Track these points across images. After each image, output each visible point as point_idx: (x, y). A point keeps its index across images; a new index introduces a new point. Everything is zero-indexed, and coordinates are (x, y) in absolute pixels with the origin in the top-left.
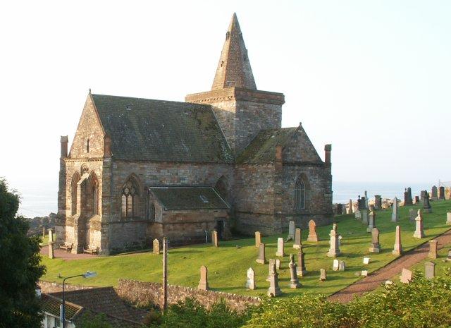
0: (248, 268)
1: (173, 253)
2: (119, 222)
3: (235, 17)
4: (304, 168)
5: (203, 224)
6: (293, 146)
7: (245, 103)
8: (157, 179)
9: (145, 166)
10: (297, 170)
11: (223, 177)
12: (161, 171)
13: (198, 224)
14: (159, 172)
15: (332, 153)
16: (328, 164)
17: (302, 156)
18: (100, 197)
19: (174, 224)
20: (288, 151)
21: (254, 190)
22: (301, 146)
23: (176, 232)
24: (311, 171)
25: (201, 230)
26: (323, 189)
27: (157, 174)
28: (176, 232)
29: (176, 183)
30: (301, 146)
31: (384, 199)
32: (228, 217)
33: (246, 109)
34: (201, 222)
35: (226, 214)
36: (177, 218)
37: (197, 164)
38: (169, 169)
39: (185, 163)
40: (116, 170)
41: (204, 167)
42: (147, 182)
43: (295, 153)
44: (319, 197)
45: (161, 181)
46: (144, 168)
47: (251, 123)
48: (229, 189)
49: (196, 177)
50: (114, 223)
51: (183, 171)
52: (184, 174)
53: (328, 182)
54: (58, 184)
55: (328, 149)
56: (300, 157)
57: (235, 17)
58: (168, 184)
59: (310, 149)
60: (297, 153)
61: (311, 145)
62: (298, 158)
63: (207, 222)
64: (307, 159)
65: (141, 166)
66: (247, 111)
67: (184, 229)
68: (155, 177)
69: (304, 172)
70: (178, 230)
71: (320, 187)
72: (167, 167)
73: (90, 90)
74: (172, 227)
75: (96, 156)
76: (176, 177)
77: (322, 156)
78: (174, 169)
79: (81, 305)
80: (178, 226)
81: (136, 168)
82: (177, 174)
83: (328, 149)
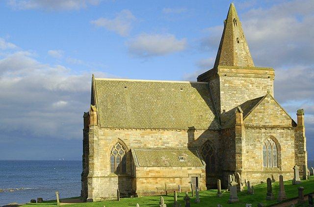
0: (251, 193)
2: (106, 177)
5: (176, 179)
10: (265, 133)
12: (145, 136)
13: (172, 179)
14: (143, 137)
17: (272, 121)
20: (255, 116)
23: (149, 185)
24: (282, 134)
25: (175, 184)
28: (149, 185)
29: (160, 146)
34: (174, 178)
35: (201, 172)
36: (150, 173)
37: (176, 129)
38: (152, 135)
40: (102, 135)
45: (146, 145)
48: (216, 152)
49: (180, 141)
58: (152, 147)
63: (181, 178)
67: (157, 183)
70: (144, 183)
74: (145, 181)
75: (272, 204)
76: (160, 141)
78: (158, 134)
80: (151, 180)
81: (122, 134)
82: (161, 139)
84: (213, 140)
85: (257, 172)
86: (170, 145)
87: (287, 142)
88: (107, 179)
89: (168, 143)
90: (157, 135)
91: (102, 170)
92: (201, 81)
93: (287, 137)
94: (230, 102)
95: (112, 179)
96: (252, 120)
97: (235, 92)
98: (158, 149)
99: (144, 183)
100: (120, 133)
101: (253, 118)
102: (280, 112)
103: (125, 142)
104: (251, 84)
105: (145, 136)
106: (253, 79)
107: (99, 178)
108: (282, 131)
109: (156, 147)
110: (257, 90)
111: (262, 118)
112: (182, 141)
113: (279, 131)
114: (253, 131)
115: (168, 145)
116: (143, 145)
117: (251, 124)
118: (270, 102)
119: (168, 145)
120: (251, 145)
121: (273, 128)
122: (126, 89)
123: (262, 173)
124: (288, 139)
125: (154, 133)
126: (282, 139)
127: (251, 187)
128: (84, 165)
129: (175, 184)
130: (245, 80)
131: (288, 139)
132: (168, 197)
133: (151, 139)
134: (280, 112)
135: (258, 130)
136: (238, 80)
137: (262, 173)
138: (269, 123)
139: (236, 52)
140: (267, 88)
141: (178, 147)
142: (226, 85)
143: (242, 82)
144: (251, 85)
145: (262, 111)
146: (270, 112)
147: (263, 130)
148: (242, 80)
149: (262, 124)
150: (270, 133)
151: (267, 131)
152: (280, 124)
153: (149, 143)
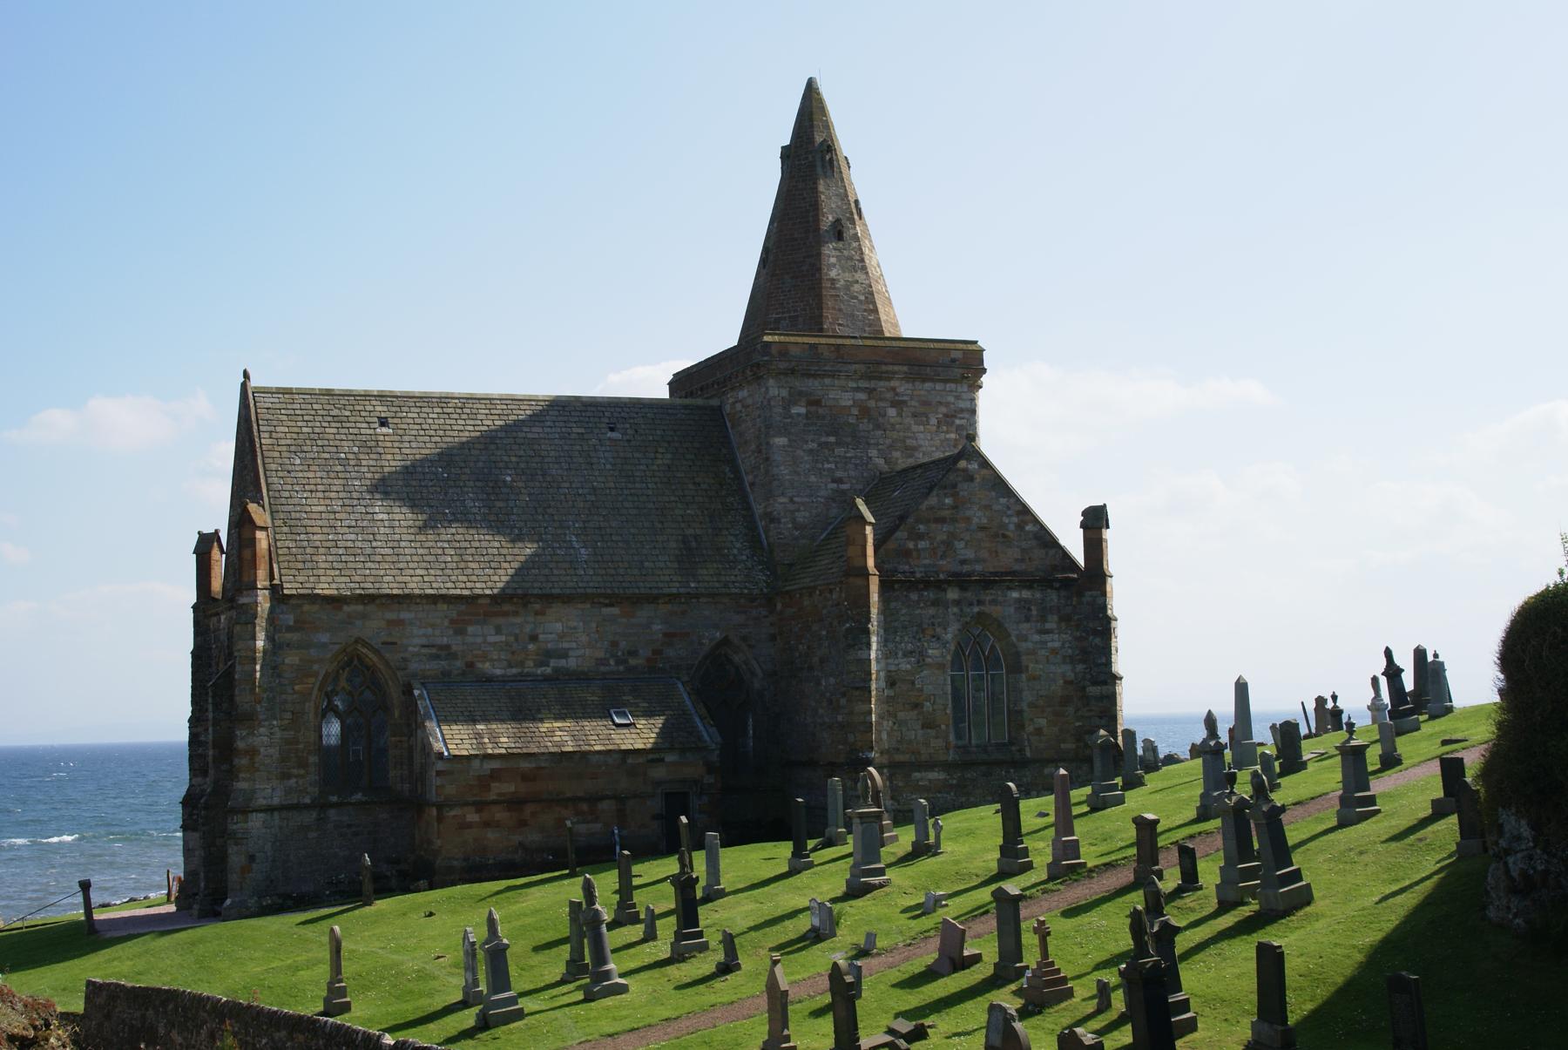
1: (905, 866)
2: (306, 807)
3: (811, 110)
4: (987, 596)
5: (605, 805)
6: (942, 520)
7: (813, 385)
8: (452, 656)
9: (405, 615)
10: (957, 603)
11: (725, 641)
12: (470, 629)
13: (585, 807)
14: (461, 632)
15: (1112, 537)
16: (1094, 575)
17: (984, 554)
19: (480, 806)
20: (920, 537)
21: (818, 683)
22: (978, 517)
24: (1023, 605)
25: (597, 827)
26: (1080, 667)
27: (456, 644)
28: (491, 835)
30: (978, 517)
31: (1213, 711)
32: (709, 779)
37: (612, 600)
38: (500, 620)
39: (567, 599)
40: (289, 629)
41: (644, 613)
42: (414, 666)
43: (948, 544)
44: (1065, 701)
45: (471, 665)
46: (400, 622)
47: (839, 451)
48: (757, 685)
49: (614, 644)
50: (281, 808)
51: (559, 627)
52: (562, 636)
54: (190, 691)
55: (1095, 520)
56: (969, 553)
57: (811, 110)
58: (498, 672)
59: (1020, 527)
60: (959, 545)
61: (1025, 511)
62: (963, 562)
64: (1008, 558)
65: (391, 616)
67: (523, 823)
68: (445, 652)
69: (987, 609)
71: (1071, 660)
73: (246, 375)
74: (472, 817)
76: (531, 647)
77: (1073, 543)
80: (500, 814)
82: (534, 638)
83: (1095, 520)
84: (744, 639)
85: (929, 765)
86: (572, 663)
87: (1046, 637)
88: (310, 817)
89: (564, 654)
90: (518, 620)
91: (285, 776)
92: (691, 395)
93: (1043, 619)
94: (813, 478)
95: (332, 813)
96: (907, 554)
97: (832, 439)
98: (521, 678)
99: (470, 826)
100: (364, 616)
101: (911, 545)
103: (387, 655)
104: (894, 404)
105: (470, 629)
106: (903, 388)
107: (276, 814)
108: (1026, 594)
109: (514, 671)
110: (915, 428)
112: (623, 644)
114: (914, 596)
115: (562, 663)
116: (459, 663)
117: (907, 568)
118: (978, 479)
119: (562, 663)
120: (905, 655)
121: (987, 582)
122: (384, 430)
123: (947, 766)
124: (1048, 626)
125: (505, 614)
127: (1515, 874)
128: (1075, 908)
129: (597, 827)
130: (870, 391)
131: (1048, 626)
132: (404, 580)
133: (491, 639)
134: (1015, 519)
135: (930, 595)
136: (844, 389)
137: (947, 766)
138: (977, 561)
139: (833, 274)
140: (958, 422)
141: (602, 669)
142: (795, 410)
143: (862, 396)
144: (892, 412)
145: (946, 513)
147: (953, 594)
148: (858, 389)
149: (947, 565)
151: (968, 595)
152: (1017, 567)
153: (485, 658)
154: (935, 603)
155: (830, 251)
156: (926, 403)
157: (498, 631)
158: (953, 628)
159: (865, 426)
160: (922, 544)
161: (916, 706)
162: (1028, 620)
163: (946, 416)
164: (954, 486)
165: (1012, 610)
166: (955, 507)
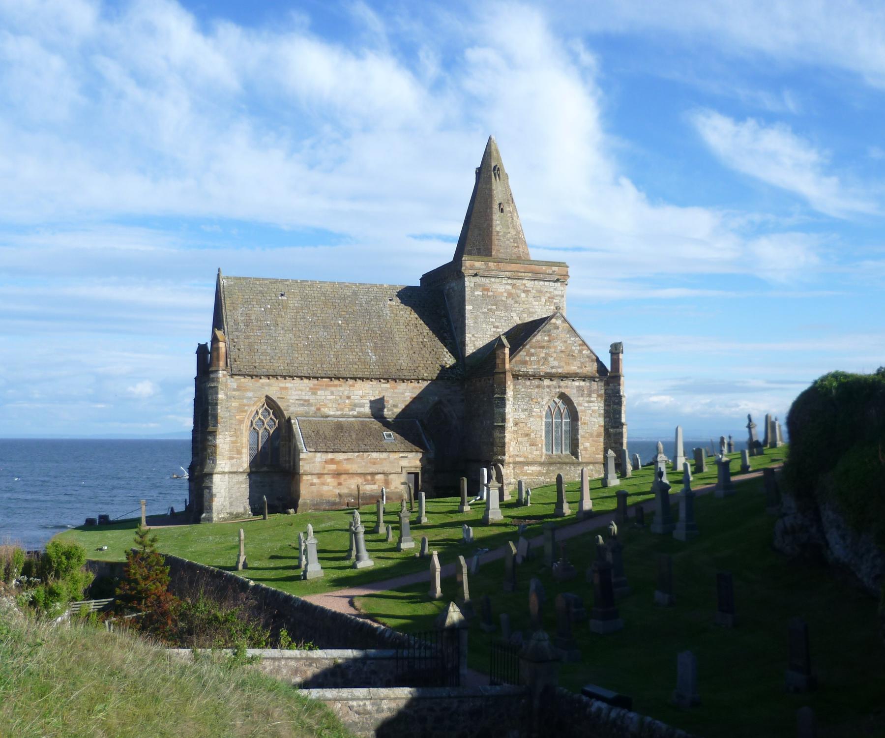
6: (543, 347)
12: (319, 392)
13: (369, 477)
14: (314, 394)
18: (426, 441)
23: (325, 488)
25: (375, 487)
29: (346, 411)
33: (488, 290)
34: (373, 474)
38: (333, 389)
43: (545, 359)
45: (319, 409)
46: (286, 388)
53: (618, 416)
55: (616, 350)
58: (332, 413)
62: (552, 368)
65: (282, 385)
66: (490, 294)
67: (340, 484)
68: (307, 403)
72: (328, 386)
79: (402, 632)
82: (349, 398)
83: (616, 350)
87: (591, 404)
93: (590, 395)
97: (494, 307)
102: (578, 348)
108: (582, 383)
111: (545, 359)
113: (577, 383)
114: (528, 383)
123: (541, 464)
126: (581, 399)
130: (513, 285)
140: (555, 301)
144: (523, 295)
146: (560, 346)
147: (547, 382)
150: (559, 387)
154: (538, 387)
155: (497, 217)
156: (540, 292)
157: (332, 394)
158: (546, 398)
159: (510, 301)
160: (533, 358)
161: (527, 435)
162: (582, 396)
163: (549, 298)
164: (549, 331)
165: (575, 391)
166: (549, 341)
